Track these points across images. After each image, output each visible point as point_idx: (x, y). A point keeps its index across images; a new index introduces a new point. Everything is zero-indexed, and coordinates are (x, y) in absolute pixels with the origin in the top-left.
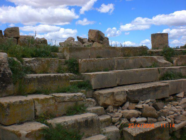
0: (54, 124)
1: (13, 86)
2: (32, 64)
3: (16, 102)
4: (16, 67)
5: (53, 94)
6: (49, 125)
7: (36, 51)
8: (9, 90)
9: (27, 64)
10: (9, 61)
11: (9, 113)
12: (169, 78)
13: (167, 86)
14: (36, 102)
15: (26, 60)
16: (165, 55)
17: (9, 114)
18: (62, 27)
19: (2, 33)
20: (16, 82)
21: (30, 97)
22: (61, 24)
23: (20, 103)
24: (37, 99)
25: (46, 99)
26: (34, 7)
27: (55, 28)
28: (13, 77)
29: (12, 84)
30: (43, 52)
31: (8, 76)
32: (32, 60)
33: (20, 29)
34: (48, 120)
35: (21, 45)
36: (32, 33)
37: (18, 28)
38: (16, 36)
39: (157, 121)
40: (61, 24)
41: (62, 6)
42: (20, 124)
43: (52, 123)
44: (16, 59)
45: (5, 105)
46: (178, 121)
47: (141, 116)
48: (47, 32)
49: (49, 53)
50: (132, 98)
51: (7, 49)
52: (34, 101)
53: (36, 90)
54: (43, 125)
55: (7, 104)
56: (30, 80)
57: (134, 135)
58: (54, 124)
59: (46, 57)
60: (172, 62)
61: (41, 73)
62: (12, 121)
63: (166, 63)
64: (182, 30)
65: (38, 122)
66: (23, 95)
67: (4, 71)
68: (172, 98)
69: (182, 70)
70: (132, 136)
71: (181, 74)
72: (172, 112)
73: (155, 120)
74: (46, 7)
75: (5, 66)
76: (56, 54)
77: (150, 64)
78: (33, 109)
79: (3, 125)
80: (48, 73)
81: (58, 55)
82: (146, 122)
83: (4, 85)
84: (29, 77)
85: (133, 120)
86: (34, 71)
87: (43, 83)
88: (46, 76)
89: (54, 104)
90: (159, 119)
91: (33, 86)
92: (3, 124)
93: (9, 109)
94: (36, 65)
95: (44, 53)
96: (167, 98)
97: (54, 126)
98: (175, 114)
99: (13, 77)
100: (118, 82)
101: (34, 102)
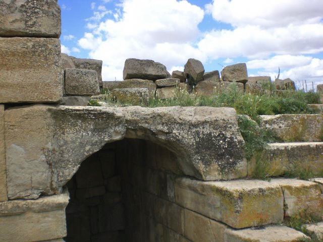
0: (320, 234)
1: (246, 164)
2: (276, 126)
3: (253, 190)
4: (250, 132)
5: (317, 180)
6: (311, 234)
7: (281, 103)
8: (239, 169)
9: (268, 126)
10: (238, 120)
11: (240, 208)
14: (286, 191)
15: (265, 120)
17: (241, 210)
18: (314, 56)
19: (218, 74)
20: (252, 156)
21: (275, 184)
22: (313, 51)
23: (260, 192)
24: (289, 188)
25: (305, 187)
26: (265, 27)
27: (301, 59)
28: (246, 148)
29: (245, 160)
30: (293, 104)
31: (238, 146)
32: (275, 119)
33: (250, 66)
34: (308, 225)
35: (255, 92)
36: (263, 71)
37: (244, 65)
38: (242, 79)
40: (313, 51)
41: (313, 20)
42: (258, 229)
43: (316, 232)
44: (248, 117)
45: (236, 195)
48: (288, 67)
49: (303, 105)
51: (233, 101)
52: (282, 189)
53: (284, 171)
54: (300, 234)
55: (238, 194)
56: (274, 154)
58: (320, 234)
59: (300, 113)
61: (291, 141)
62: (246, 223)
65: (290, 227)
66: (263, 179)
67: (231, 138)
74: (284, 25)
75: (233, 129)
76: (316, 107)
78: (282, 204)
79: (229, 227)
80: (303, 141)
81: (320, 108)
83: (231, 160)
84: (272, 148)
86: (280, 137)
87: (297, 159)
88: (302, 147)
89: (317, 197)
91: (280, 165)
92: (231, 225)
93: (242, 202)
94: (283, 126)
95: (295, 106)
97: (320, 237)
99: (246, 148)
101: (283, 193)
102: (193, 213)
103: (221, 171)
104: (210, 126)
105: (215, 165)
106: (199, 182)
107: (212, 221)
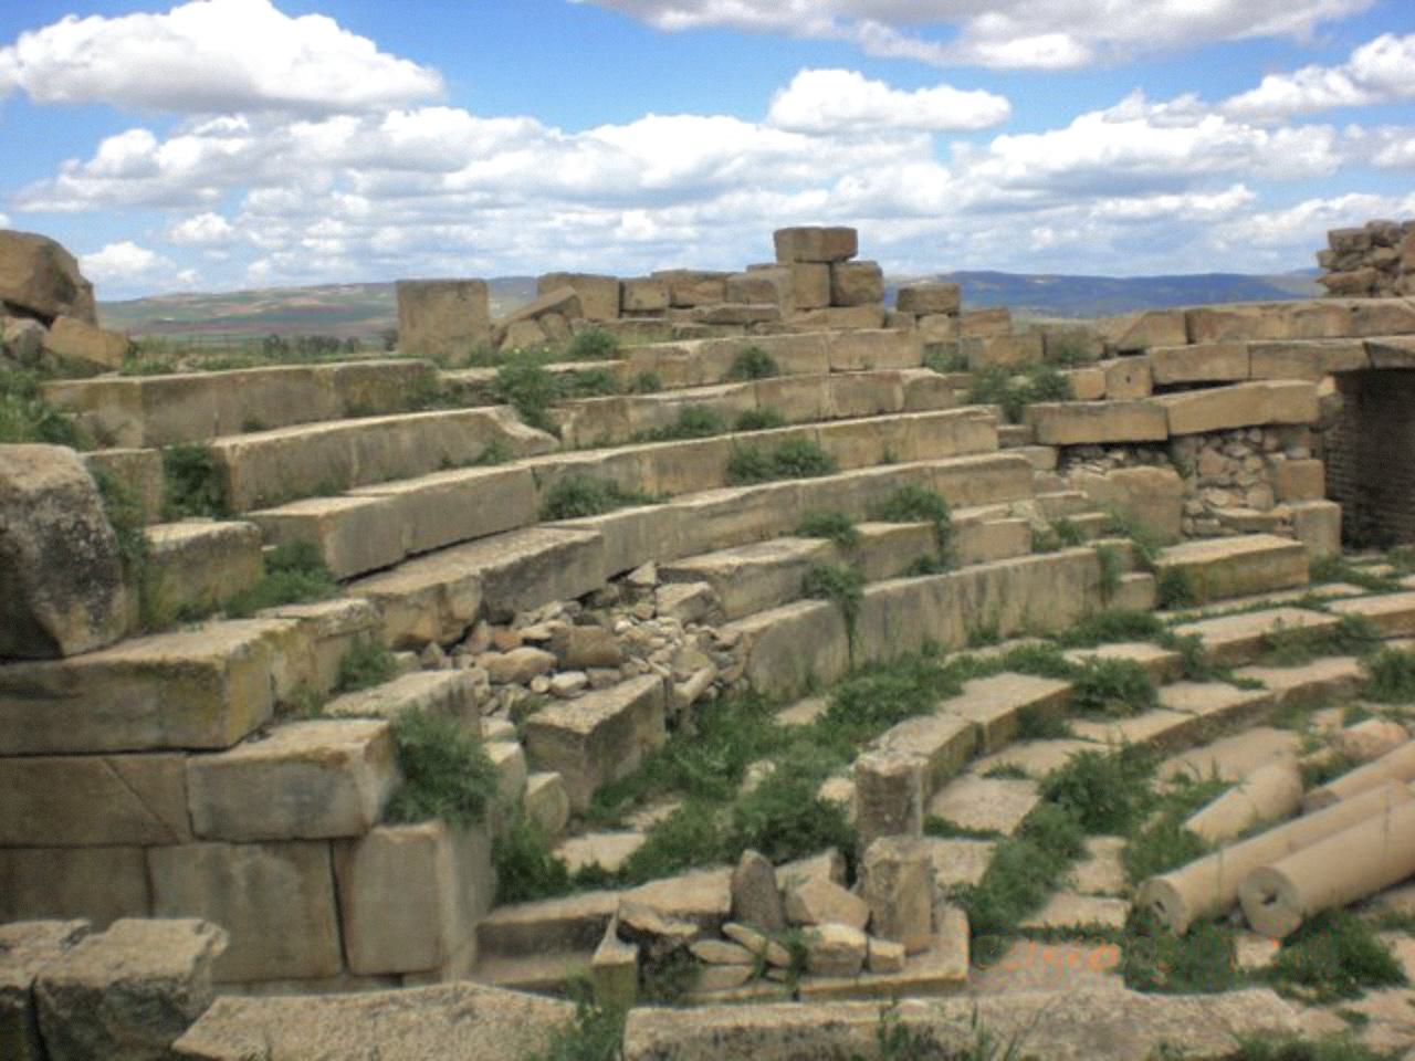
12: (580, 506)
13: (597, 541)
16: (515, 400)
39: (625, 678)
46: (684, 673)
47: (560, 668)
50: (500, 601)
57: (585, 730)
60: (557, 433)
63: (535, 440)
64: (233, 146)
68: (615, 590)
69: (615, 468)
70: (578, 736)
71: (615, 484)
72: (662, 641)
73: (615, 674)
77: (476, 448)
82: (588, 686)
85: (541, 684)
90: (627, 667)
96: (599, 591)
98: (672, 647)
100: (406, 543)
102: (16, 761)
103: (96, 624)
104: (53, 501)
105: (80, 611)
106: (47, 666)
107: (122, 759)
